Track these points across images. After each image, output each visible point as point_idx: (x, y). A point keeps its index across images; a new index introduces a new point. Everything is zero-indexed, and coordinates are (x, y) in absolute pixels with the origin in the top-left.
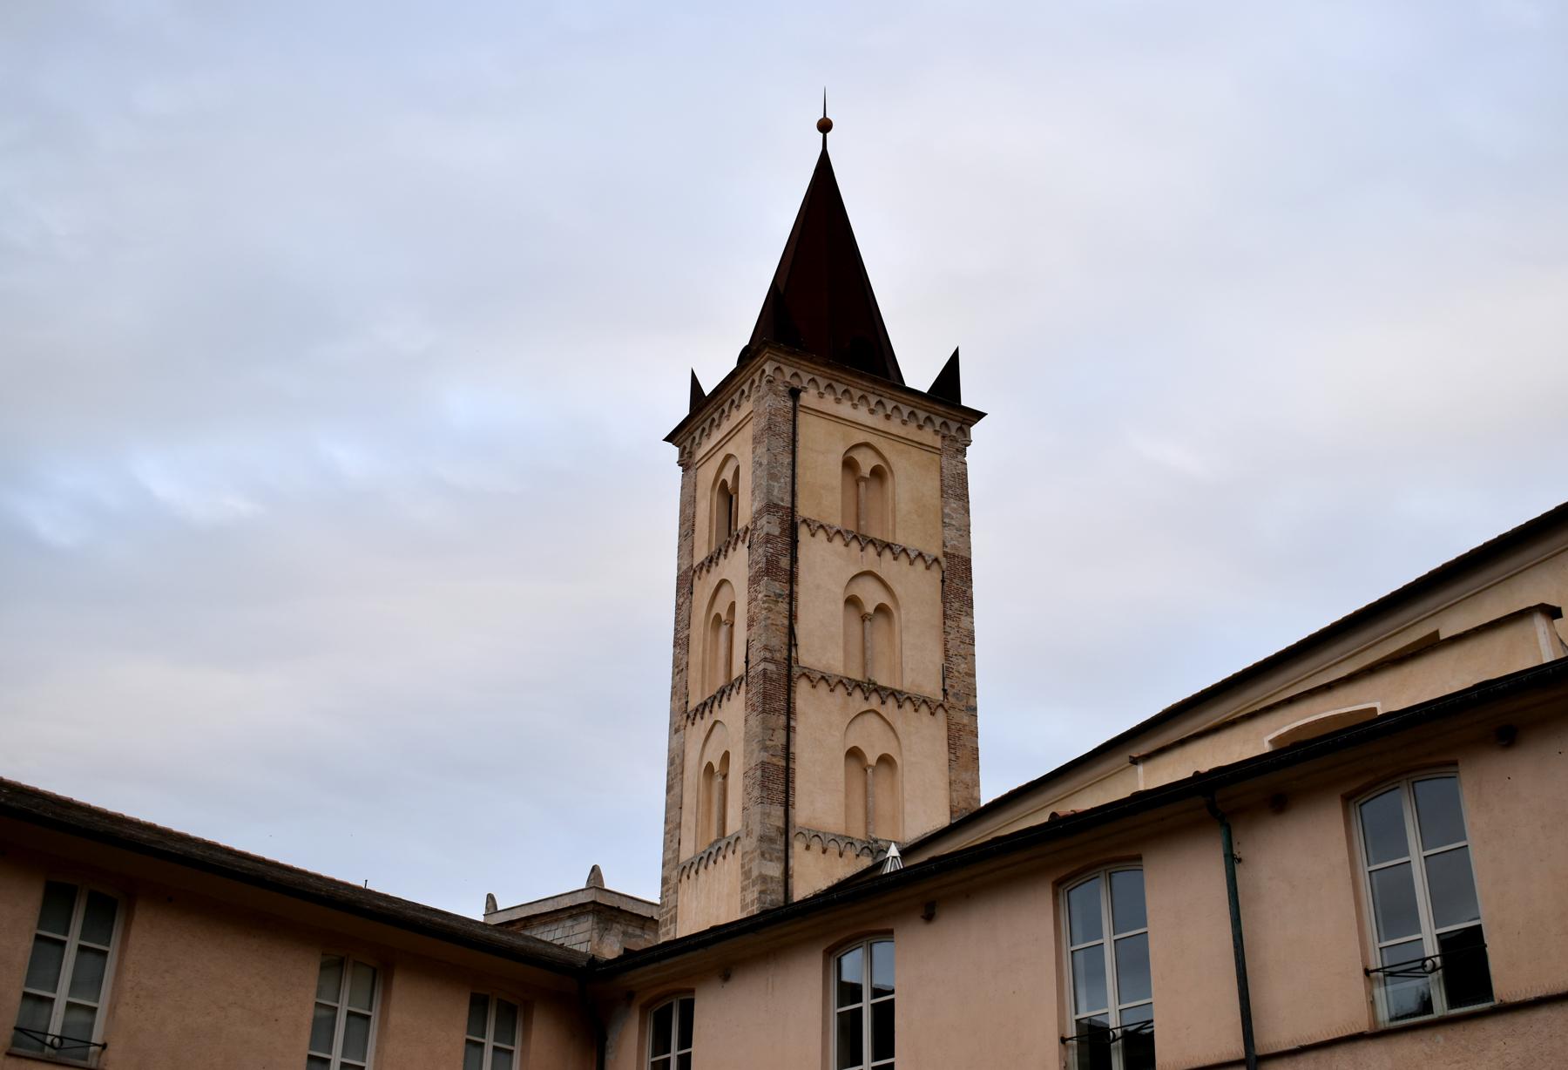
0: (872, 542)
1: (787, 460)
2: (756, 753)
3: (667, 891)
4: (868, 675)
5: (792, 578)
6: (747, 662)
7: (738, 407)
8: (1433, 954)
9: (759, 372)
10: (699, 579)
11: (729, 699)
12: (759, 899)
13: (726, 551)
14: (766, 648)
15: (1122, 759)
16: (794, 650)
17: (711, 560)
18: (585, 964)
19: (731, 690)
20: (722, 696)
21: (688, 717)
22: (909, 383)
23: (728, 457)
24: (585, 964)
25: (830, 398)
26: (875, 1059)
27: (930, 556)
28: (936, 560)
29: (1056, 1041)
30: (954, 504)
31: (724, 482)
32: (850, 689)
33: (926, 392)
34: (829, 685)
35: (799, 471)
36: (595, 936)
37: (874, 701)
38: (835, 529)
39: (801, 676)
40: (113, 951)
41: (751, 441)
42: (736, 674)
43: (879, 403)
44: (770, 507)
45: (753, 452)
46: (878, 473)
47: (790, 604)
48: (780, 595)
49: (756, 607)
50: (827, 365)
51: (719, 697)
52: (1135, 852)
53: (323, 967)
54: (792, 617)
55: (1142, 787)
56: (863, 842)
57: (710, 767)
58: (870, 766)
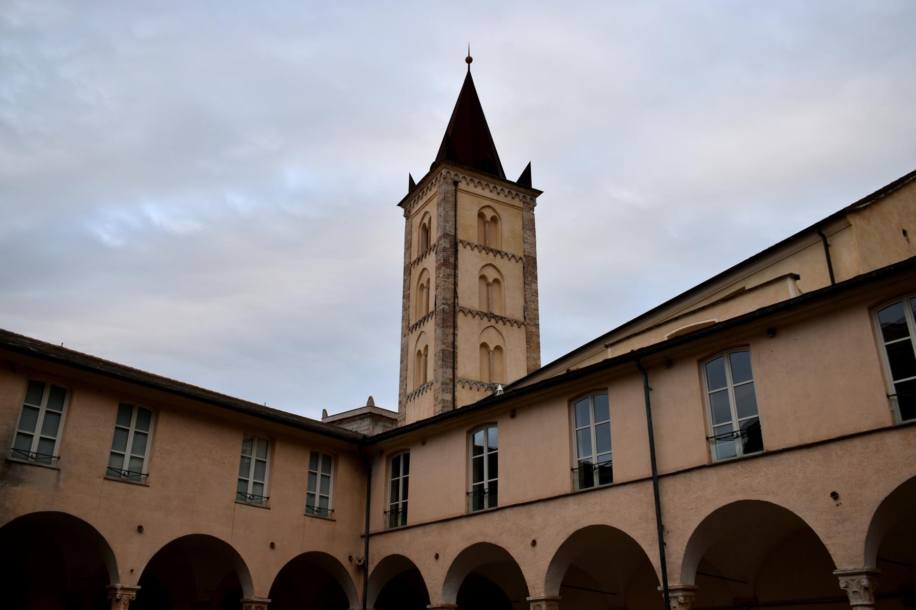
0: (491, 250)
1: (453, 213)
2: (440, 345)
3: (401, 407)
4: (490, 310)
5: (455, 267)
6: (435, 305)
7: (430, 190)
8: (737, 430)
9: (440, 174)
10: (414, 268)
11: (427, 322)
12: (442, 410)
13: (426, 255)
14: (444, 298)
15: (602, 346)
16: (456, 299)
17: (419, 259)
18: (361, 438)
19: (428, 317)
20: (424, 320)
21: (410, 330)
22: (508, 178)
23: (426, 213)
24: (361, 438)
25: (472, 185)
26: (490, 478)
27: (518, 257)
28: (521, 258)
29: (569, 470)
30: (529, 233)
31: (425, 224)
32: (482, 317)
33: (516, 182)
34: (473, 315)
35: (458, 218)
36: (371, 426)
37: (493, 322)
38: (475, 245)
39: (460, 311)
40: (64, 413)
41: (436, 205)
42: (430, 310)
43: (495, 187)
44: (445, 235)
45: (437, 210)
46: (494, 219)
47: (455, 279)
48: (450, 275)
49: (439, 280)
50: (470, 170)
51: (423, 320)
52: (604, 386)
53: (244, 441)
54: (455, 284)
55: (610, 357)
56: (488, 384)
57: (419, 351)
58: (491, 351)
